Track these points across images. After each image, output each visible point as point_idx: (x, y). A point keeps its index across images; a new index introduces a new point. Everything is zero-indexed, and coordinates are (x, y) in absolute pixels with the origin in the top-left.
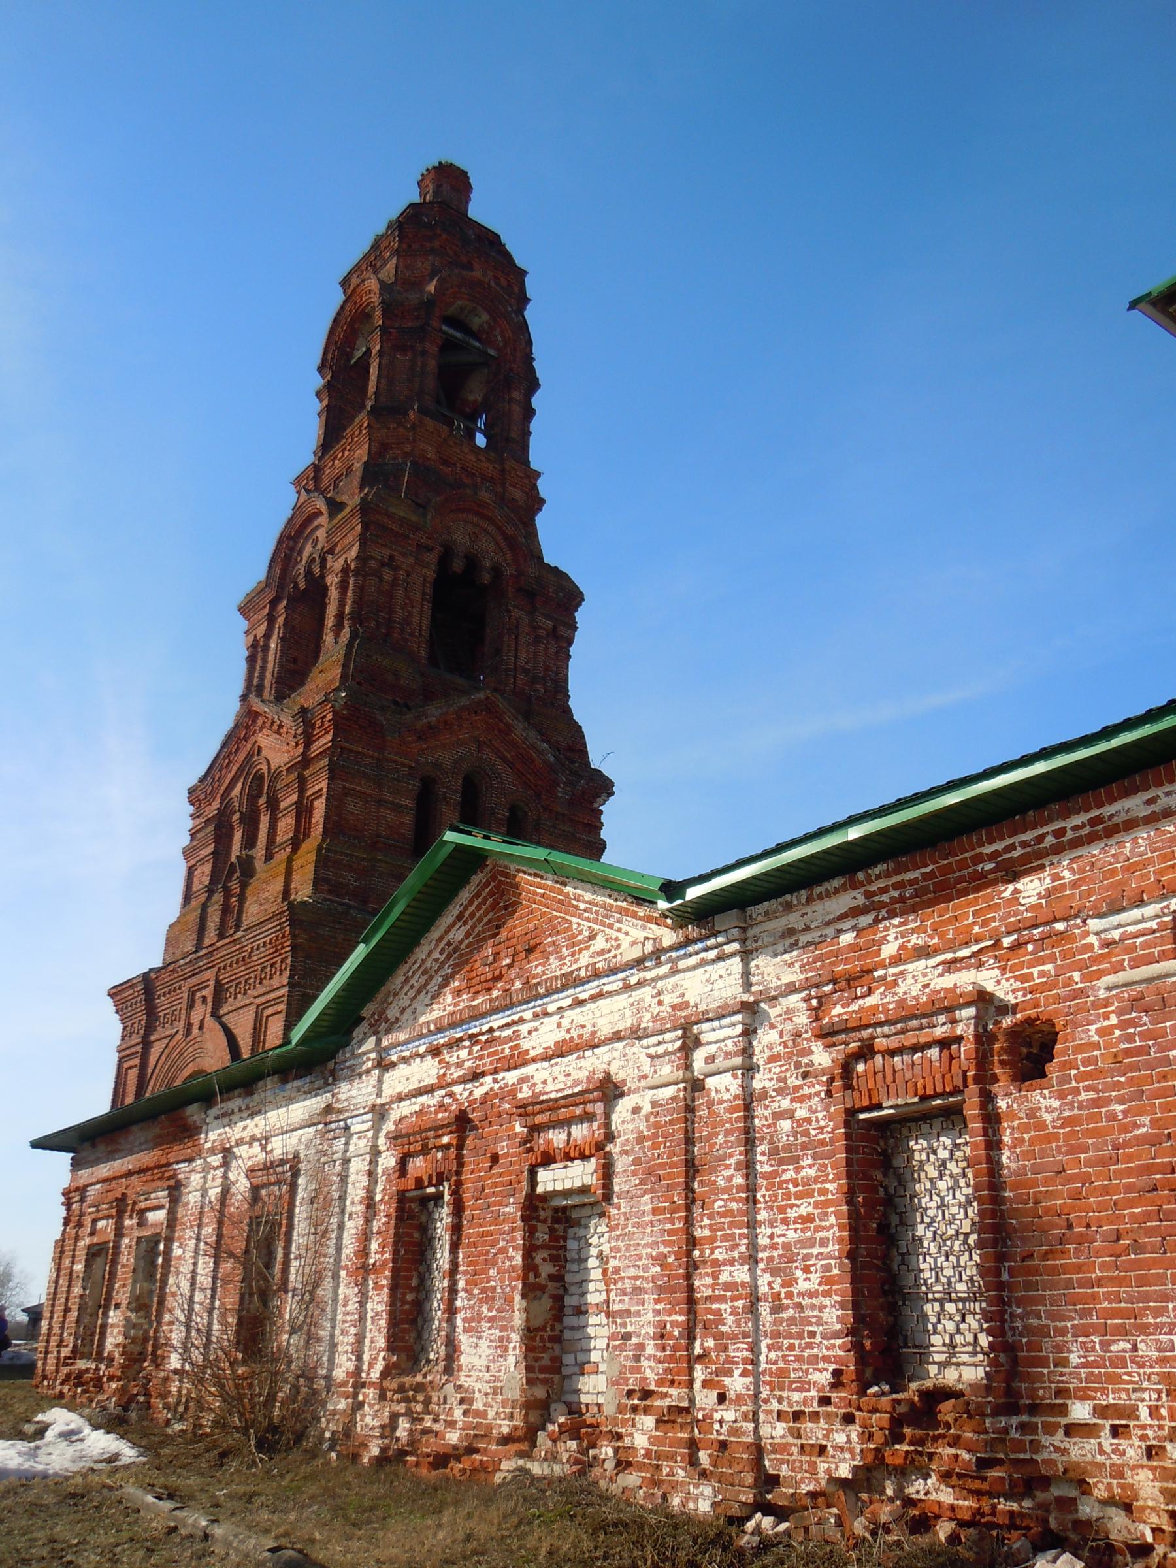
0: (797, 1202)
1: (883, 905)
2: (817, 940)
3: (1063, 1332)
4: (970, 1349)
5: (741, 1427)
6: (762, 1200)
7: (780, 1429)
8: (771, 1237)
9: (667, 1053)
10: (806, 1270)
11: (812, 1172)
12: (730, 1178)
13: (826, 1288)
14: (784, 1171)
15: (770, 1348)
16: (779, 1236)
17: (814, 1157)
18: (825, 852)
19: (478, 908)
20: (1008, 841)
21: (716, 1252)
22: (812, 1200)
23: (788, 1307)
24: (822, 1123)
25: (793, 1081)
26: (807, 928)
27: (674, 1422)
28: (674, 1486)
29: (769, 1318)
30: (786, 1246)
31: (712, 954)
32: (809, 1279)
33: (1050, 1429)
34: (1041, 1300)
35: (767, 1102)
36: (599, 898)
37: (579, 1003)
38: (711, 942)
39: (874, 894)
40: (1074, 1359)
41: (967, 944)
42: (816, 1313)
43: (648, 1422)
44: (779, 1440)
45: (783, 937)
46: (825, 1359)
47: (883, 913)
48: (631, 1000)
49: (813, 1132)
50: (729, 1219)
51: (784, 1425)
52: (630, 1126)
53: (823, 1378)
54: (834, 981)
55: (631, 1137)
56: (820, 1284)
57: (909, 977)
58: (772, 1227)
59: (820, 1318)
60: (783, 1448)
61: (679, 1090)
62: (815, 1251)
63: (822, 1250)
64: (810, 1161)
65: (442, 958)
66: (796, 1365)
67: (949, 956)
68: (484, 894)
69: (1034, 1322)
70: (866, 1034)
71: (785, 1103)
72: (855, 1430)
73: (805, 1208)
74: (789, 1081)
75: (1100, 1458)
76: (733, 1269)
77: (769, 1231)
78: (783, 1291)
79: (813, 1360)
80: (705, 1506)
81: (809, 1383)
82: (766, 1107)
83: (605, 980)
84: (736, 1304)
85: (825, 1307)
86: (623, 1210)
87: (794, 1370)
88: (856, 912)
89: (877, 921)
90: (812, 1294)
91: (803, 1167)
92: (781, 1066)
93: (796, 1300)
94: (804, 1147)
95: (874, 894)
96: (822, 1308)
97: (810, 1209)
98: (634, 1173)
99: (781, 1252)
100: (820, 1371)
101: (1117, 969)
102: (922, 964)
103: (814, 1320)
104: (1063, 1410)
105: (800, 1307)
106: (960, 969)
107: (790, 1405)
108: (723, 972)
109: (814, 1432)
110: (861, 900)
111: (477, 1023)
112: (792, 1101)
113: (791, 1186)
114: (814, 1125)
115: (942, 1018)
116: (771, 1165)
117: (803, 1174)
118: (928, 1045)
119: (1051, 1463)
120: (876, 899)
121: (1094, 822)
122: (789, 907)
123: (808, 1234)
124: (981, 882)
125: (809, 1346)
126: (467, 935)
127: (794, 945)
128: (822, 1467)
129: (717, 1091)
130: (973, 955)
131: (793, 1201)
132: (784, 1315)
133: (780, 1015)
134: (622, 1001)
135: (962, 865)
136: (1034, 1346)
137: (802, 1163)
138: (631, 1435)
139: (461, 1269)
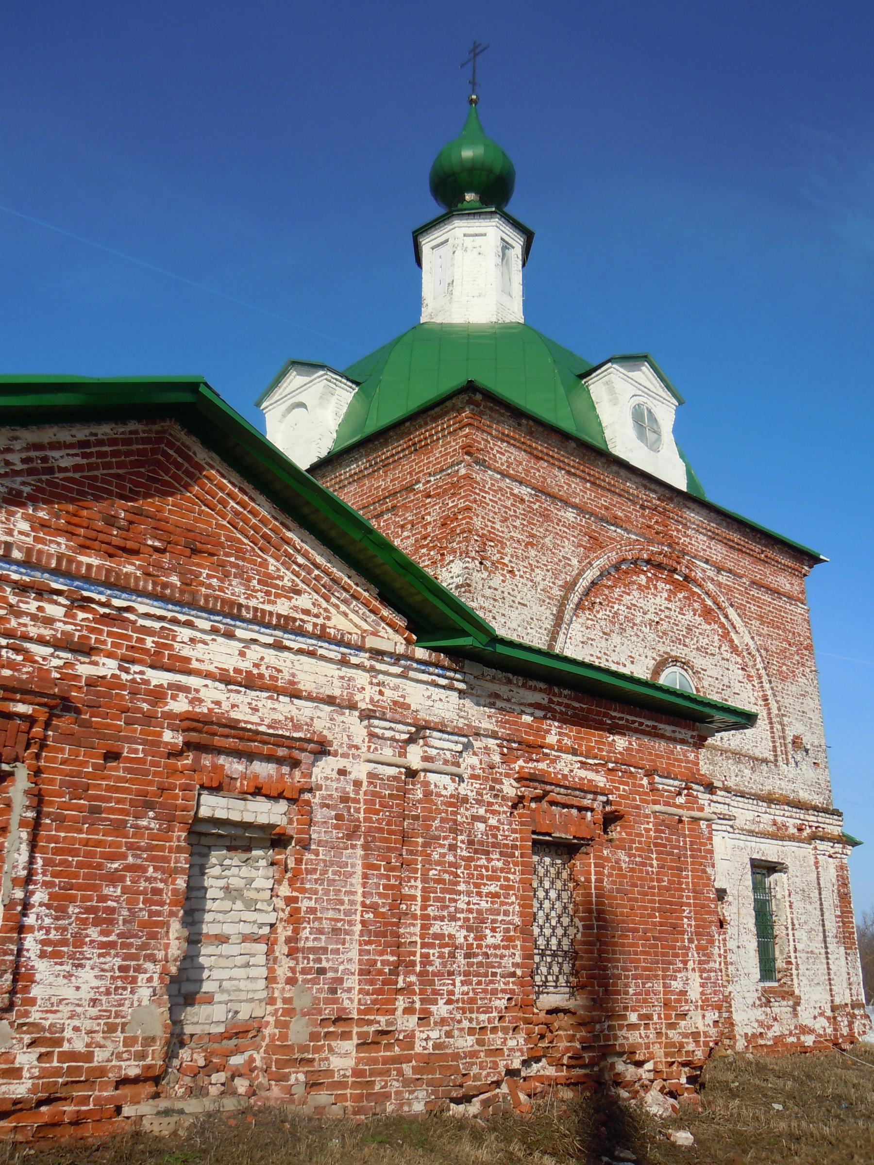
0: (489, 883)
1: (555, 711)
2: (508, 709)
3: (627, 977)
4: (554, 984)
5: (444, 1042)
6: (462, 875)
7: (471, 1040)
8: (468, 903)
9: (393, 739)
10: (493, 930)
11: (500, 864)
12: (443, 855)
13: (506, 943)
14: (479, 859)
15: (463, 983)
16: (474, 904)
17: (501, 854)
18: (654, 698)
19: (114, 454)
20: (622, 715)
21: (429, 909)
22: (499, 883)
23: (478, 955)
24: (507, 833)
25: (487, 798)
26: (508, 700)
27: (378, 1043)
28: (387, 1096)
29: (463, 961)
30: (479, 912)
31: (443, 682)
32: (495, 937)
33: (621, 1027)
34: (618, 961)
35: (468, 806)
36: (335, 570)
37: (278, 646)
38: (451, 674)
39: (553, 703)
40: (631, 991)
41: (595, 758)
42: (498, 960)
43: (349, 1046)
44: (469, 1049)
45: (490, 696)
46: (504, 991)
47: (549, 715)
48: (342, 674)
49: (500, 837)
50: (441, 886)
51: (472, 1037)
52: (335, 785)
53: (502, 1003)
54: (520, 743)
55: (336, 794)
56: (502, 941)
57: (563, 761)
58: (469, 896)
59: (501, 963)
60: (473, 1054)
61: (400, 773)
62: (500, 918)
63: (505, 918)
64: (498, 856)
65: (19, 467)
66: (482, 995)
67: (584, 760)
68: (135, 447)
69: (616, 972)
70: (548, 788)
71: (482, 811)
72: (521, 1038)
73: (493, 888)
74: (485, 797)
75: (640, 1040)
76: (442, 923)
77: (467, 899)
78: (475, 943)
79: (494, 992)
80: (418, 1107)
81: (491, 1008)
82: (467, 809)
83: (326, 645)
84: (443, 950)
85: (505, 956)
86: (321, 857)
87: (481, 999)
88: (537, 706)
89: (545, 717)
90: (496, 947)
91: (492, 859)
92: (481, 784)
93: (484, 950)
94: (494, 845)
95: (553, 703)
96: (502, 957)
97: (498, 889)
98: (336, 827)
99: (475, 915)
100: (500, 999)
101: (655, 802)
102: (570, 757)
103: (496, 965)
104: (624, 1017)
105: (486, 955)
106: (589, 770)
107: (478, 1023)
108: (443, 697)
109: (496, 1040)
110: (545, 702)
111: (109, 592)
112: (486, 811)
113: (483, 870)
114: (501, 833)
115: (590, 796)
116: (469, 852)
117: (493, 863)
118: (572, 806)
119: (622, 1045)
120: (553, 706)
121: (655, 727)
122: (509, 682)
123: (496, 906)
124: (600, 726)
125: (492, 982)
126: (77, 468)
127: (492, 705)
128: (501, 1064)
129: (436, 786)
130: (596, 764)
131: (485, 881)
132: (475, 960)
133: (480, 748)
134: (332, 670)
135: (598, 713)
136: (615, 984)
137: (491, 856)
138: (327, 1059)
139: (39, 878)
